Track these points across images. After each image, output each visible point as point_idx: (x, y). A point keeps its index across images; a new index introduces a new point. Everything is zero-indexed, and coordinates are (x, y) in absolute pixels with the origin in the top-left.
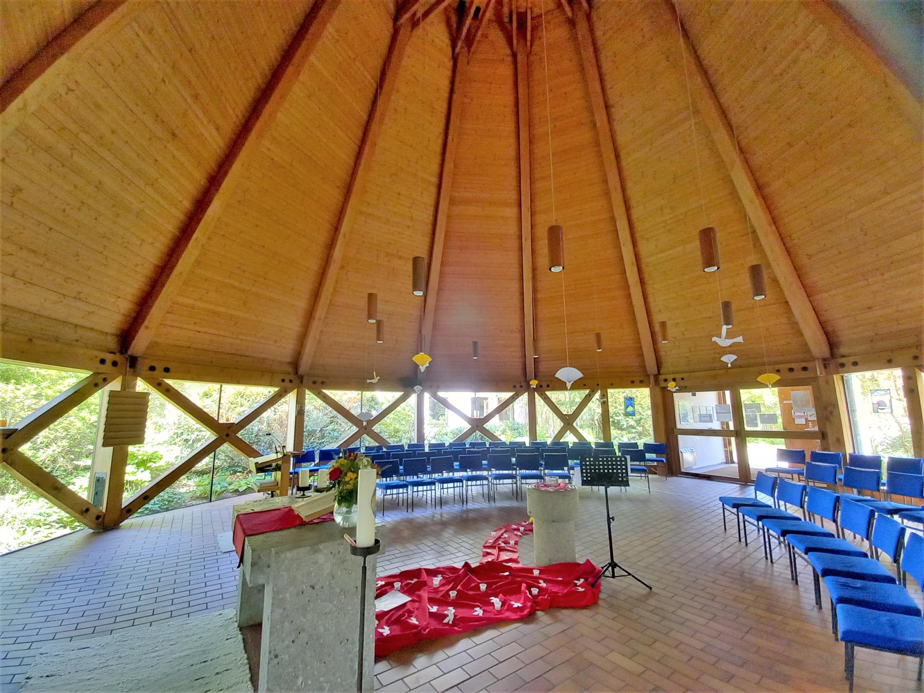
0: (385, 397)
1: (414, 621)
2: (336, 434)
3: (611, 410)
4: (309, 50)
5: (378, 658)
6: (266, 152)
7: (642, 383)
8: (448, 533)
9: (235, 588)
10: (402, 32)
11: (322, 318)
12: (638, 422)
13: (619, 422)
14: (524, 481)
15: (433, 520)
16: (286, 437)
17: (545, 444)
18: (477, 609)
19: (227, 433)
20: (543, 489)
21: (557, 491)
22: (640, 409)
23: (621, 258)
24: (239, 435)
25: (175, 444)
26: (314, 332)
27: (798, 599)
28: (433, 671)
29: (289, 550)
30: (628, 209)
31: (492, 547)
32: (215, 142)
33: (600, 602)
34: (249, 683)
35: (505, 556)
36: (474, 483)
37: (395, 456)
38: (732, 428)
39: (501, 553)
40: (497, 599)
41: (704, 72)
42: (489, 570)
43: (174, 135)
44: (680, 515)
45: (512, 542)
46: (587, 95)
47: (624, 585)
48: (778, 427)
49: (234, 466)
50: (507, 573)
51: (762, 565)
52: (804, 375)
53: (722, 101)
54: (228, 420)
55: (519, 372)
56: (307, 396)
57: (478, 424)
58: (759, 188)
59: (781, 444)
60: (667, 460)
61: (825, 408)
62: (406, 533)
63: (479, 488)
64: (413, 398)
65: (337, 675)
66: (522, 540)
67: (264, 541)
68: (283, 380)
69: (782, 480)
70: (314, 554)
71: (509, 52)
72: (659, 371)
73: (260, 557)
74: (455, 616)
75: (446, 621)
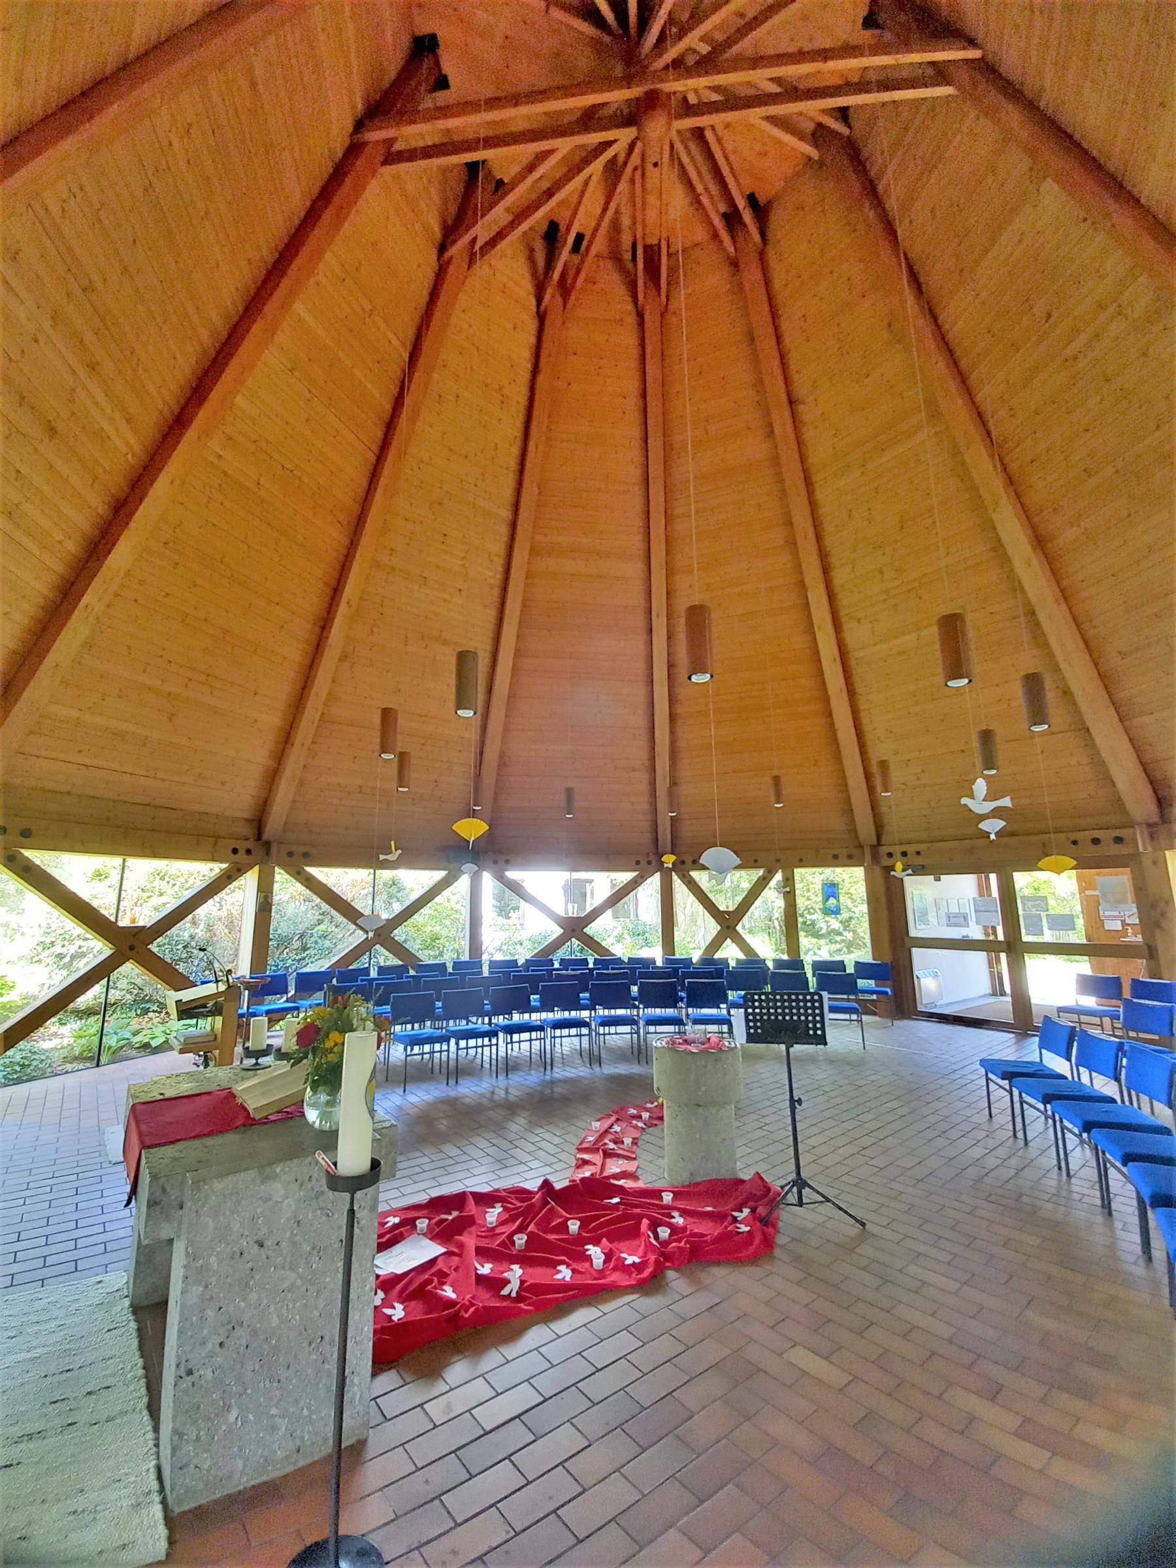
0: (416, 881)
1: (449, 1292)
2: (327, 943)
3: (801, 902)
4: (292, 294)
5: (383, 1360)
6: (216, 461)
7: (851, 860)
8: (516, 1126)
9: (129, 1231)
10: (452, 269)
11: (308, 743)
12: (846, 924)
13: (813, 924)
14: (652, 1029)
15: (491, 1100)
16: (237, 950)
17: (687, 962)
18: (562, 1268)
19: (130, 943)
20: (684, 1047)
21: (705, 1051)
22: (849, 902)
23: (816, 651)
24: (153, 947)
25: (40, 961)
26: (292, 766)
27: (1112, 1247)
28: (479, 1390)
29: (221, 1176)
30: (826, 570)
31: (592, 1150)
32: (126, 444)
33: (777, 1252)
34: (145, 1412)
35: (614, 1167)
36: (565, 1032)
37: (429, 985)
38: (1001, 937)
39: (608, 1161)
40: (598, 1250)
41: (949, 350)
42: (587, 1194)
43: (52, 431)
44: (916, 1090)
45: (628, 1141)
46: (759, 385)
47: (820, 1219)
48: (1077, 936)
49: (143, 1001)
50: (616, 1200)
51: (1051, 1182)
52: (1116, 850)
53: (979, 398)
54: (133, 921)
55: (647, 838)
56: (277, 877)
57: (575, 928)
58: (1040, 541)
59: (1084, 966)
60: (893, 990)
61: (1153, 906)
62: (443, 1125)
63: (576, 1040)
64: (463, 883)
65: (302, 1404)
66: (646, 1137)
67: (175, 1159)
68: (235, 851)
69: (1084, 1032)
70: (262, 1183)
71: (630, 307)
72: (879, 839)
73: (164, 1190)
74: (522, 1282)
75: (505, 1292)
